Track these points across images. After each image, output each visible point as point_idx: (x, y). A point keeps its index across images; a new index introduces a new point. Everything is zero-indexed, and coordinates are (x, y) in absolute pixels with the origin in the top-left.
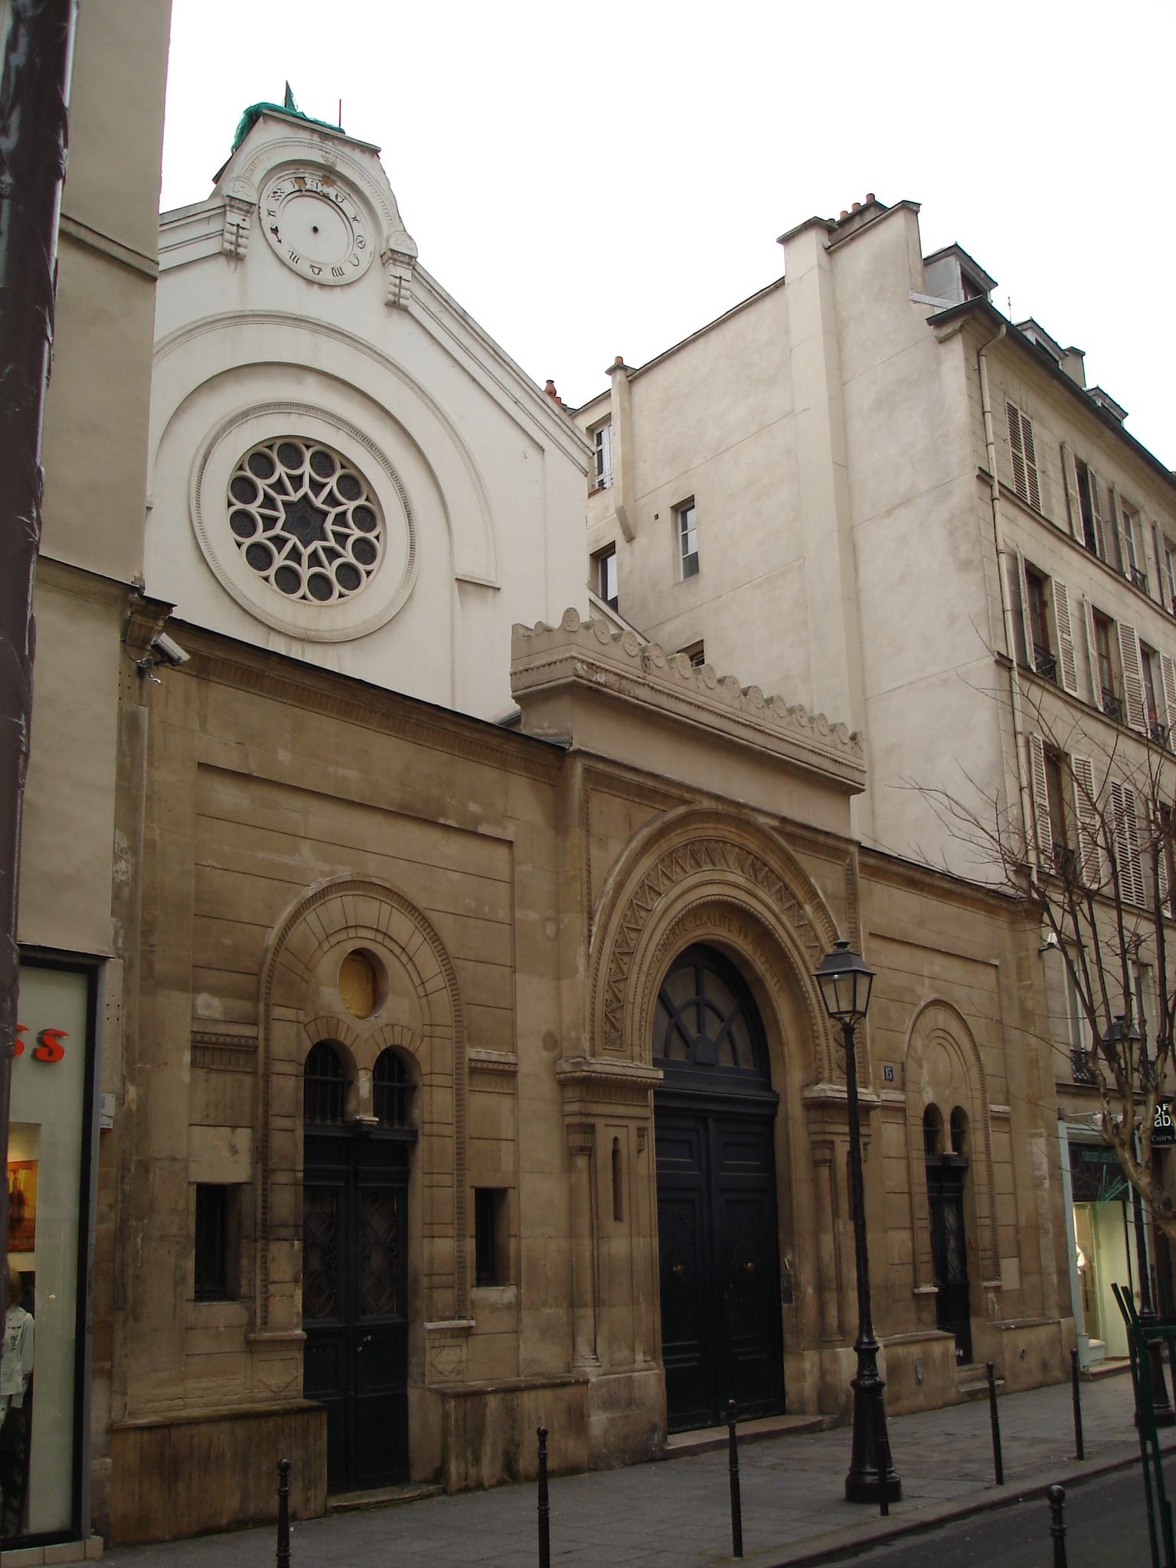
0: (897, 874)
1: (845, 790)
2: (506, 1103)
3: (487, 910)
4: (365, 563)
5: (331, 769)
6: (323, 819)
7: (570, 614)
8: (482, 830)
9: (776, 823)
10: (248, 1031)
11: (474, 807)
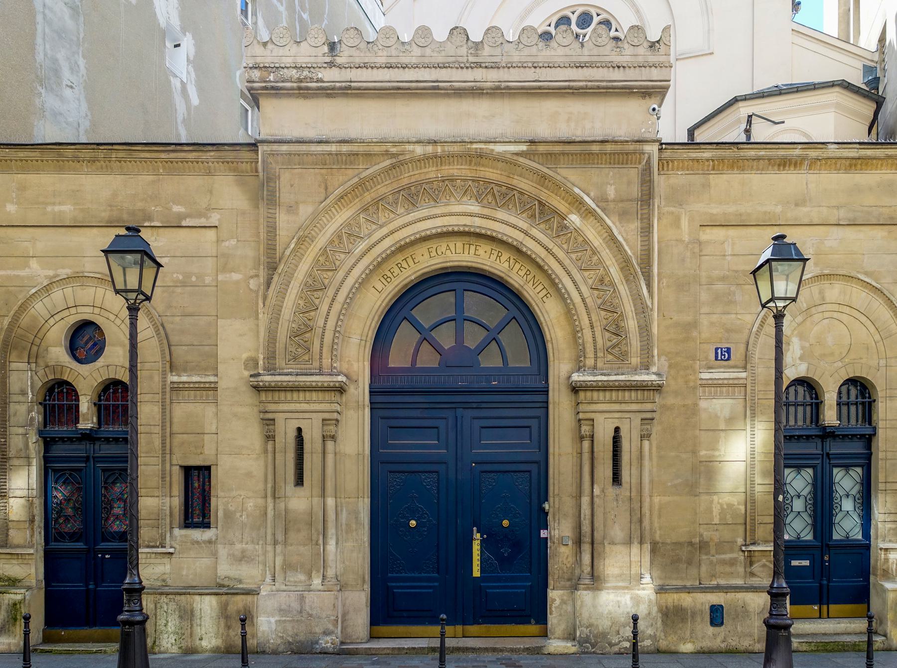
0: (758, 159)
1: (654, 92)
2: (210, 410)
3: (194, 279)
5: (49, 209)
6: (46, 240)
7: (424, 32)
8: (184, 224)
9: (523, 148)
11: (177, 209)
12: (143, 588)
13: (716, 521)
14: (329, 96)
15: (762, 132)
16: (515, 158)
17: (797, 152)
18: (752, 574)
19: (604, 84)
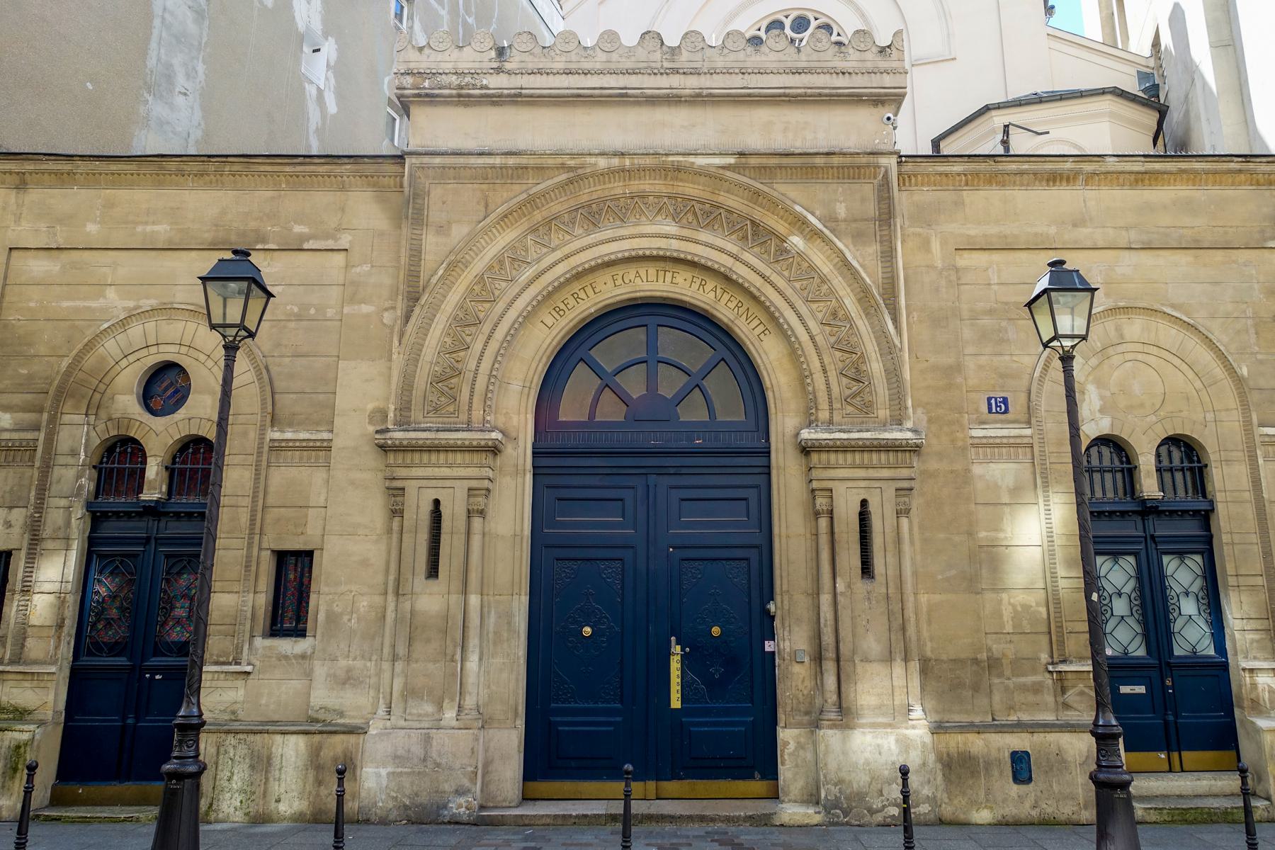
0: (1022, 173)
1: (890, 100)
4: (809, 22)
8: (306, 246)
9: (732, 160)
10: (29, 435)
11: (298, 229)
12: (204, 723)
13: (1009, 628)
14: (494, 104)
15: (1021, 143)
16: (721, 171)
17: (1069, 165)
18: (1066, 706)
19: (827, 91)
